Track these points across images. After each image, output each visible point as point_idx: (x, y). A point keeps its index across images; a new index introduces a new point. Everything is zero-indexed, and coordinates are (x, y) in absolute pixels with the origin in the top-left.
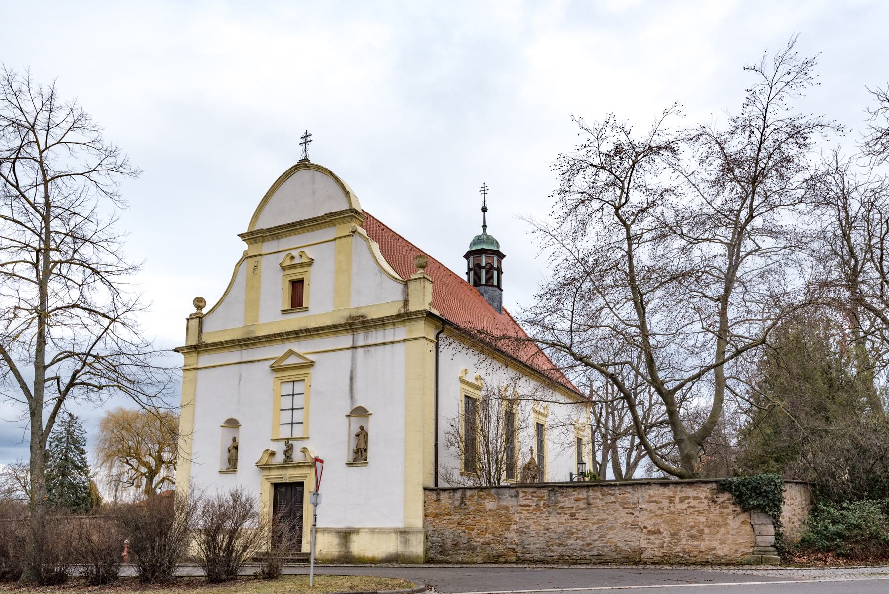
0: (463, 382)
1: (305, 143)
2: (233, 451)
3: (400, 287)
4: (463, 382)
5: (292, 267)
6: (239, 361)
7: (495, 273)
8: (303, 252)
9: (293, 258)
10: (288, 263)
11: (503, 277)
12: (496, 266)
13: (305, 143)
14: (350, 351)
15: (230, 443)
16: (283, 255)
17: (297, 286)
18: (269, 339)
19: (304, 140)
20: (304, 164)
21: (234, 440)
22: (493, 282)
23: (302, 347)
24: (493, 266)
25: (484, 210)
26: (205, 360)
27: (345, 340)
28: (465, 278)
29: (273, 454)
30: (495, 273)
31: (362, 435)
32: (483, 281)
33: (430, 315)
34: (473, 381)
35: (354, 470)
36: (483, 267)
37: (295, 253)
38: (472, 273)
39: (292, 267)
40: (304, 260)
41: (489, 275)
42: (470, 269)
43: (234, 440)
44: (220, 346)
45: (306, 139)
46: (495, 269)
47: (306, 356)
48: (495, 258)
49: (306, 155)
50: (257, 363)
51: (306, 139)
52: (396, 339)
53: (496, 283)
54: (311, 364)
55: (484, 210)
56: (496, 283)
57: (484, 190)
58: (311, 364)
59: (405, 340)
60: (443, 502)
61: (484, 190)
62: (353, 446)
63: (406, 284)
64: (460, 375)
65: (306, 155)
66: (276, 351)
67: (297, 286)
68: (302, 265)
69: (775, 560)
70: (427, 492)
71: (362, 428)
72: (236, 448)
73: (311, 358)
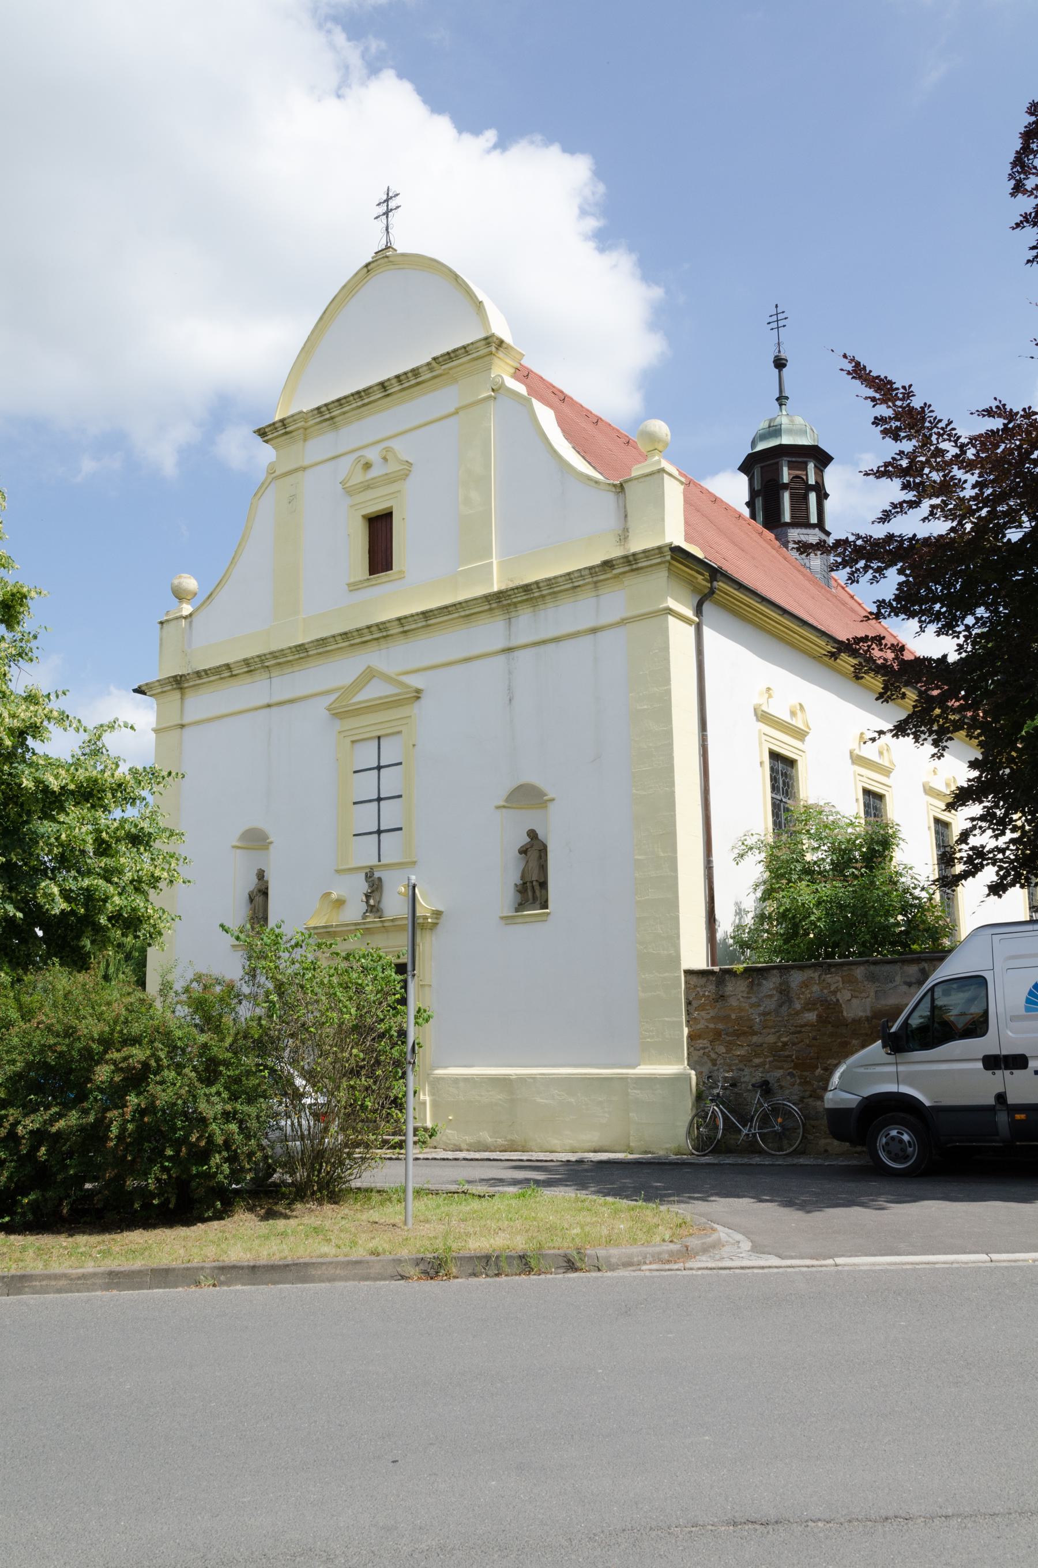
0: (763, 717)
1: (386, 214)
2: (259, 899)
3: (610, 499)
4: (763, 717)
5: (368, 486)
6: (265, 701)
7: (813, 497)
8: (388, 449)
9: (368, 466)
10: (359, 477)
11: (828, 504)
12: (812, 481)
13: (386, 214)
14: (502, 658)
15: (252, 883)
16: (347, 462)
17: (380, 528)
18: (321, 648)
19: (383, 208)
20: (385, 258)
21: (261, 875)
22: (808, 517)
23: (393, 659)
24: (806, 482)
25: (780, 364)
26: (200, 704)
27: (490, 633)
28: (746, 512)
29: (340, 903)
30: (813, 497)
31: (535, 850)
32: (787, 517)
33: (678, 552)
34: (786, 717)
35: (520, 931)
36: (785, 487)
37: (373, 455)
38: (759, 502)
39: (368, 486)
40: (392, 467)
41: (800, 502)
42: (753, 493)
43: (261, 875)
44: (226, 672)
45: (388, 205)
46: (811, 488)
47: (405, 679)
48: (811, 466)
49: (388, 241)
50: (296, 705)
51: (388, 205)
52: (604, 621)
53: (814, 519)
54: (417, 695)
55: (780, 364)
56: (814, 519)
57: (777, 321)
58: (417, 695)
59: (623, 622)
60: (733, 1002)
61: (777, 321)
62: (514, 877)
63: (620, 489)
64: (757, 700)
65: (388, 241)
66: (339, 672)
67: (380, 528)
68: (390, 479)
69: (946, 993)
70: (689, 977)
71: (533, 834)
72: (264, 893)
73: (415, 681)
